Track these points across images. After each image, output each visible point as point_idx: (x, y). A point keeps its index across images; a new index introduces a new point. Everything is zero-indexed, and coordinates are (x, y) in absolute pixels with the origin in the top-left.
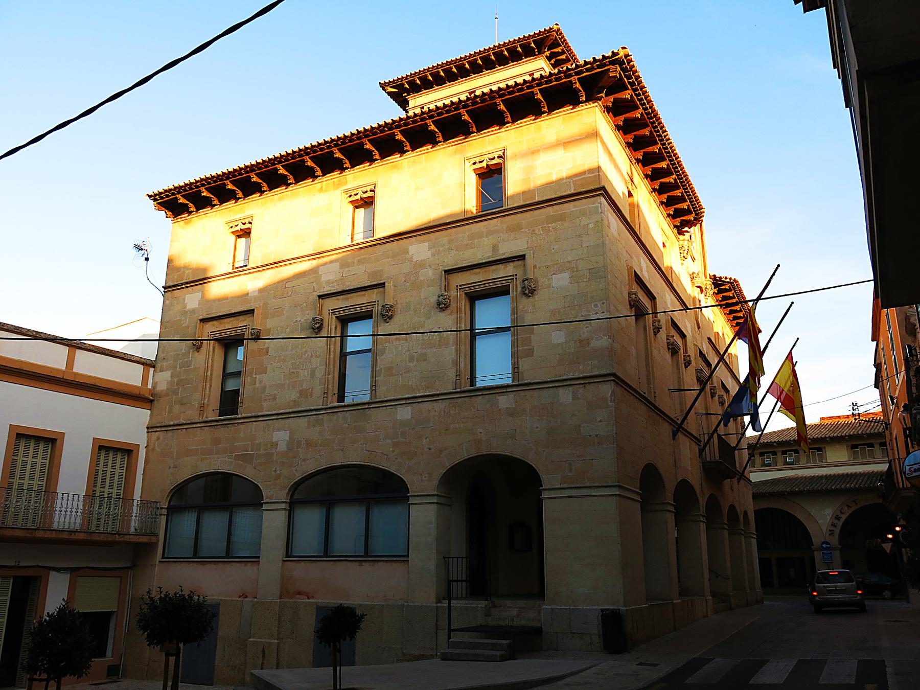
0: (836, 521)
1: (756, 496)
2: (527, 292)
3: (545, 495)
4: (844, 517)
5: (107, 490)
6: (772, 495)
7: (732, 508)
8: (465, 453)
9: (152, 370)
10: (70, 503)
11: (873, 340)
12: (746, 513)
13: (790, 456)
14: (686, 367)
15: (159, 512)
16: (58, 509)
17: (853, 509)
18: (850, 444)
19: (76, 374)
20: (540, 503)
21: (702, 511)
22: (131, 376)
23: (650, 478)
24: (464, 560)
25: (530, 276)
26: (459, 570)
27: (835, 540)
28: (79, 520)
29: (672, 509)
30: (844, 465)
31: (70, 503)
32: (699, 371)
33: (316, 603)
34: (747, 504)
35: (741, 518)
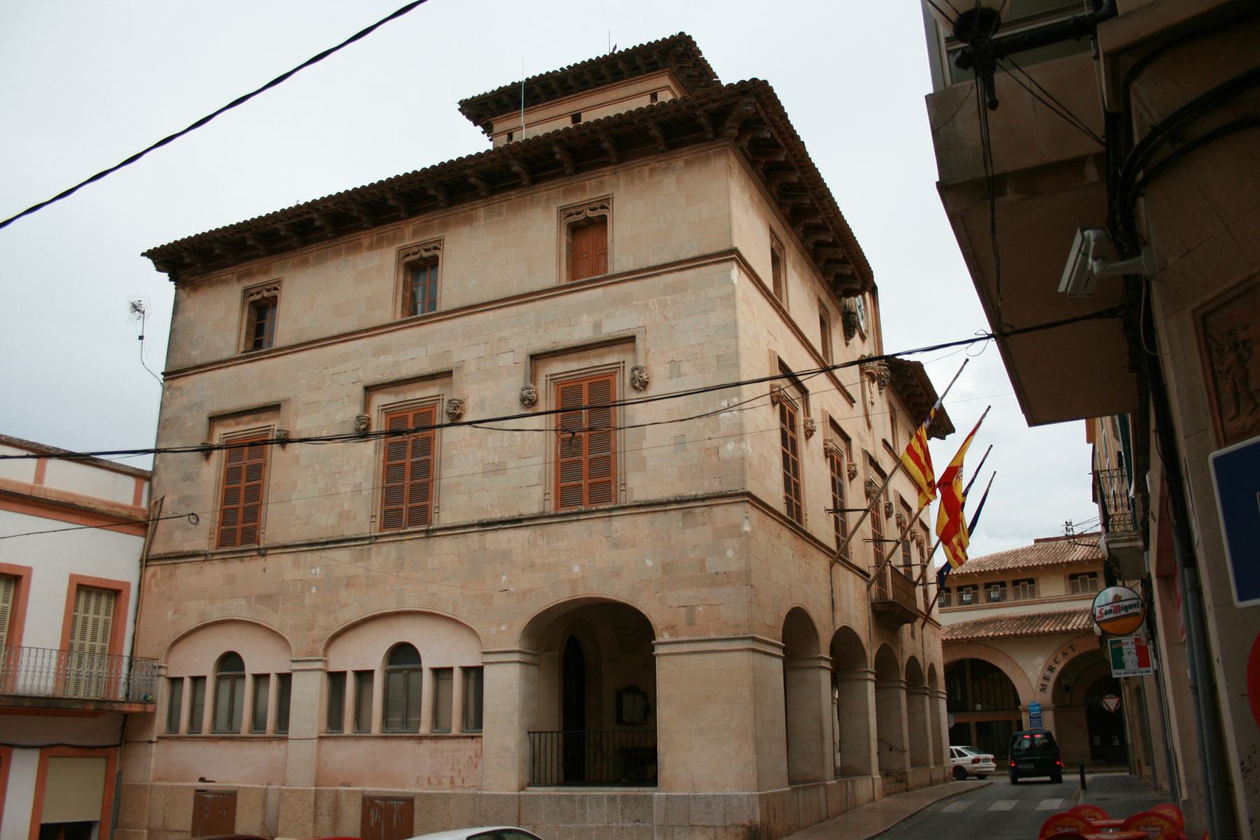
0: (1048, 673)
1: (947, 644)
2: (637, 384)
3: (659, 650)
4: (1059, 668)
5: (88, 643)
6: (971, 642)
7: (913, 661)
8: (564, 595)
9: (146, 485)
10: (39, 660)
11: (1088, 441)
12: (932, 667)
13: (995, 590)
14: (851, 479)
15: (155, 673)
16: (23, 668)
17: (1071, 655)
18: (1068, 573)
19: (46, 490)
20: (653, 658)
21: (871, 666)
22: (117, 492)
23: (797, 626)
24: (555, 735)
25: (641, 363)
26: (553, 747)
27: (1047, 698)
28: (51, 683)
29: (828, 665)
30: (1060, 600)
31: (39, 660)
32: (869, 483)
33: (362, 792)
34: (935, 656)
35: (926, 673)
